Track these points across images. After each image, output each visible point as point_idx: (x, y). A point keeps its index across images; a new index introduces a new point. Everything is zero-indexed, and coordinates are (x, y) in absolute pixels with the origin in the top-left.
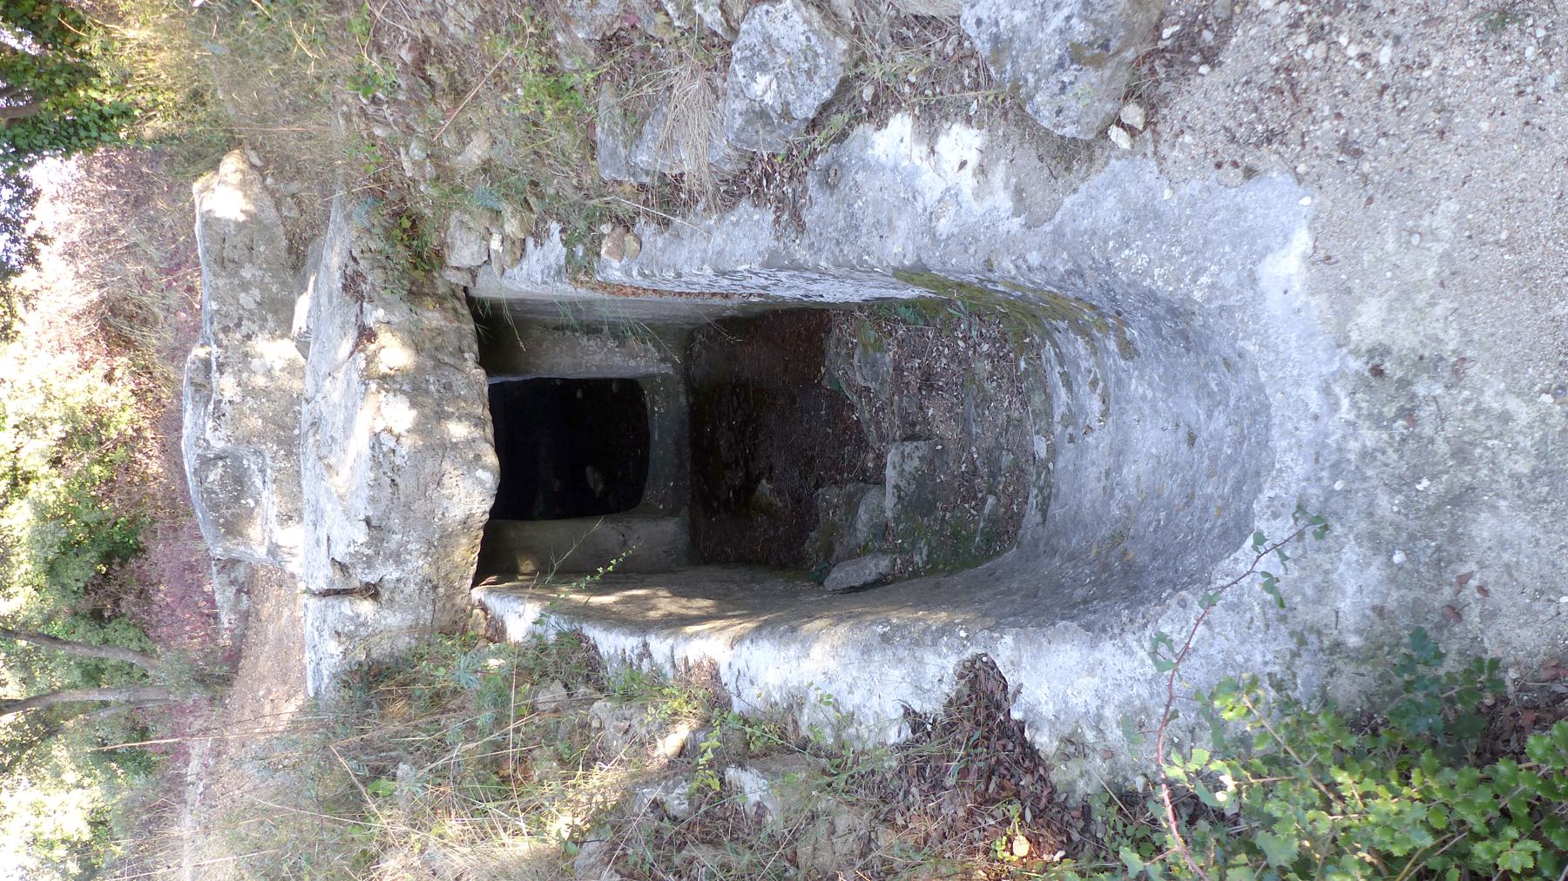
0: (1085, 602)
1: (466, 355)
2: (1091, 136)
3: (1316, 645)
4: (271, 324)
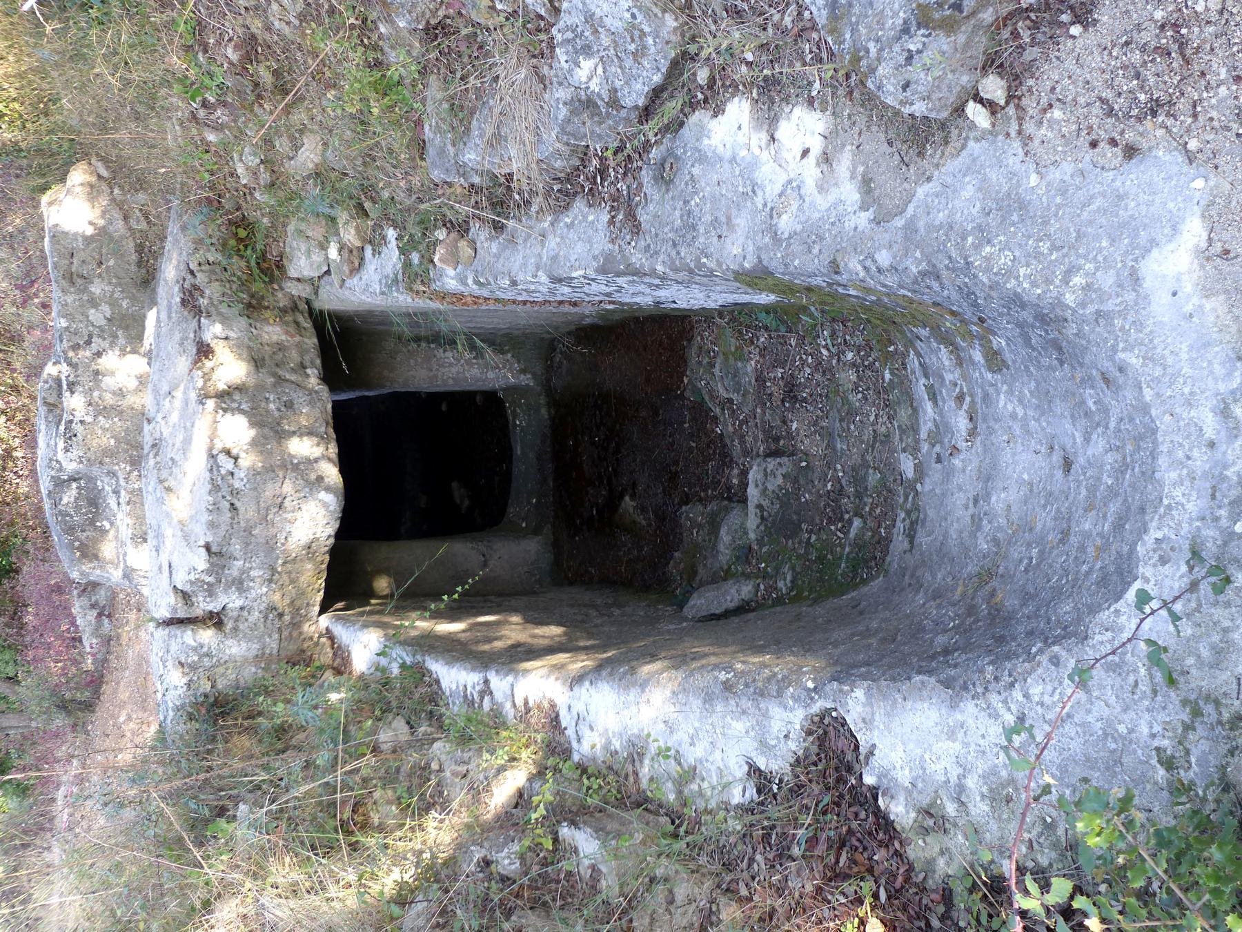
0: (946, 652)
1: (309, 371)
2: (945, 114)
3: (1214, 718)
4: (122, 341)
